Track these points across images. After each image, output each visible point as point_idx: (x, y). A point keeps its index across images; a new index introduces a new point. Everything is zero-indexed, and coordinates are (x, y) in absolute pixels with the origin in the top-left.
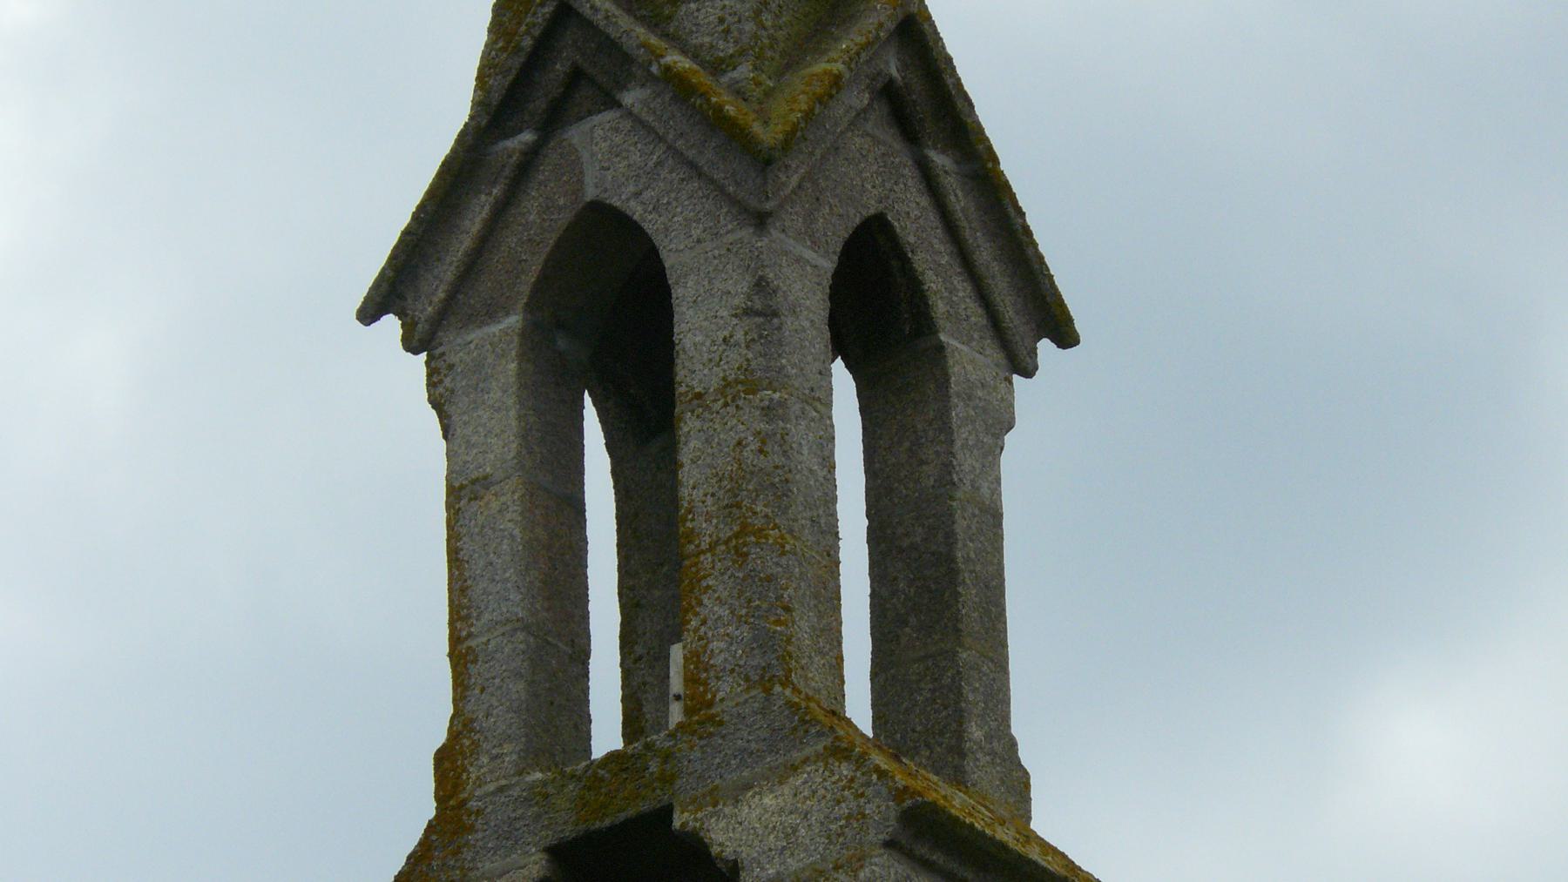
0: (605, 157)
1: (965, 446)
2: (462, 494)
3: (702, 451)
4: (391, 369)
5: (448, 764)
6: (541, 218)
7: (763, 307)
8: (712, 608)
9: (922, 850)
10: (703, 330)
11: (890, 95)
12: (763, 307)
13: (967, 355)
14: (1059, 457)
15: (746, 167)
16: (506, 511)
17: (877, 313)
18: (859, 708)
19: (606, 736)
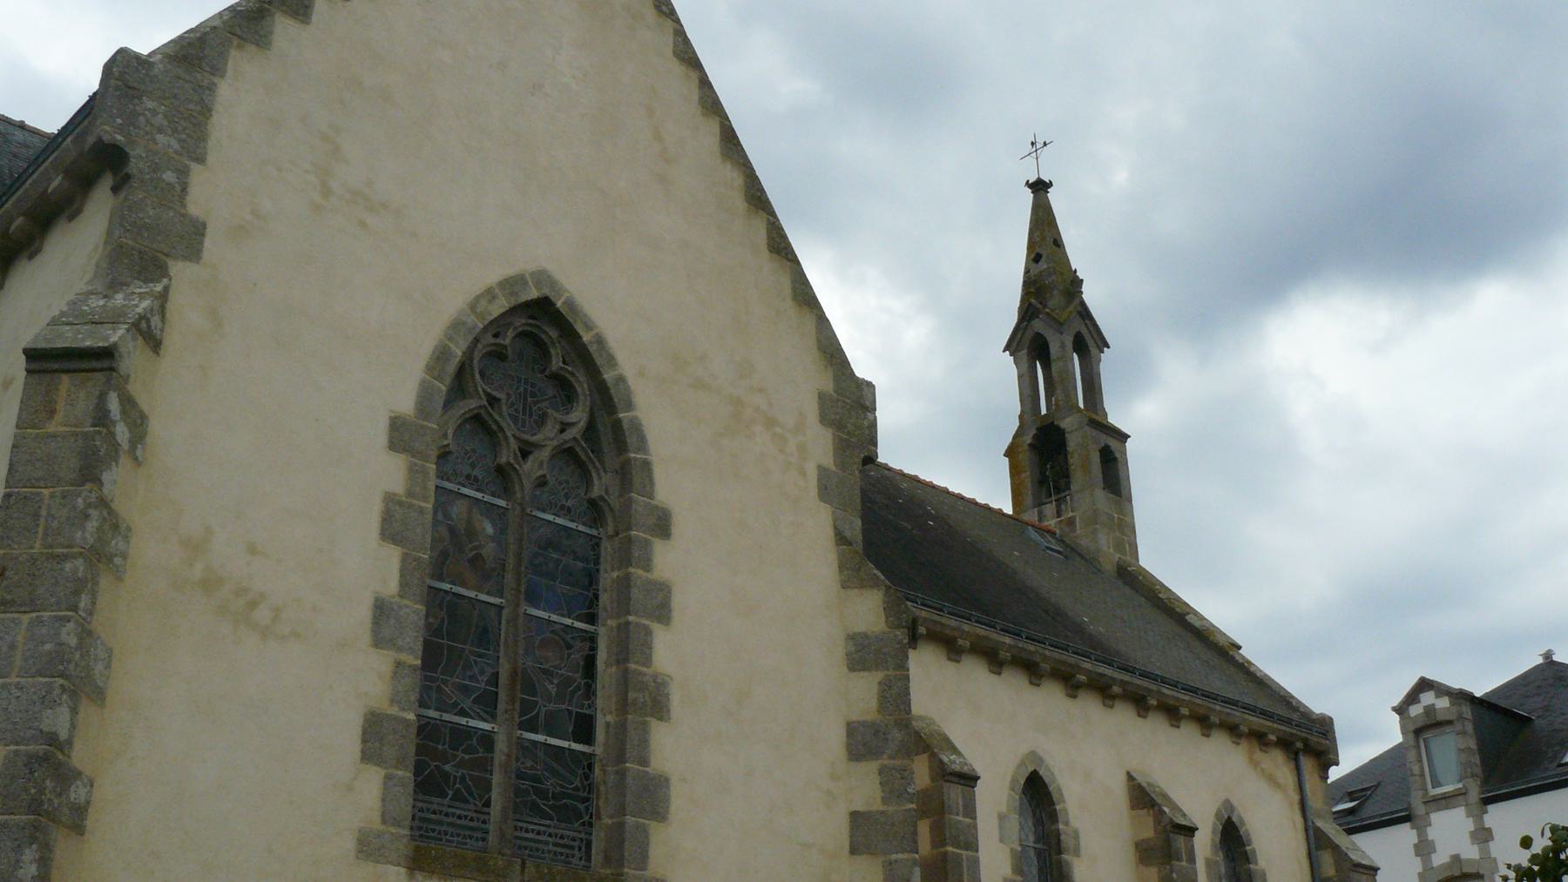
0: (1038, 325)
1: (605, 609)
2: (1020, 377)
3: (1055, 367)
4: (1008, 358)
5: (1021, 417)
6: (1029, 335)
7: (1063, 346)
8: (1059, 391)
9: (494, 427)
10: (1054, 349)
11: (1080, 313)
12: (1063, 346)
13: (1094, 350)
14: (1108, 365)
15: (1059, 325)
16: (1027, 379)
17: (1080, 346)
18: (1081, 405)
19: (1044, 411)
